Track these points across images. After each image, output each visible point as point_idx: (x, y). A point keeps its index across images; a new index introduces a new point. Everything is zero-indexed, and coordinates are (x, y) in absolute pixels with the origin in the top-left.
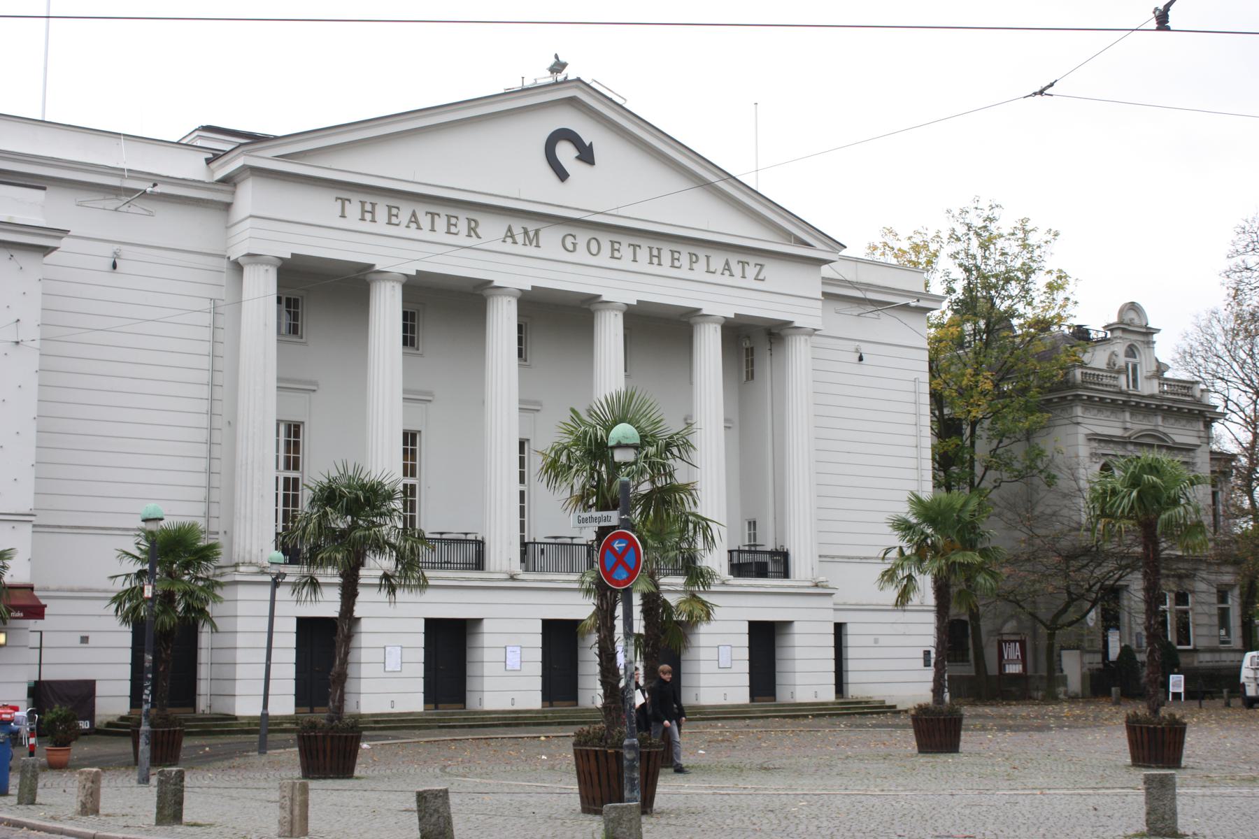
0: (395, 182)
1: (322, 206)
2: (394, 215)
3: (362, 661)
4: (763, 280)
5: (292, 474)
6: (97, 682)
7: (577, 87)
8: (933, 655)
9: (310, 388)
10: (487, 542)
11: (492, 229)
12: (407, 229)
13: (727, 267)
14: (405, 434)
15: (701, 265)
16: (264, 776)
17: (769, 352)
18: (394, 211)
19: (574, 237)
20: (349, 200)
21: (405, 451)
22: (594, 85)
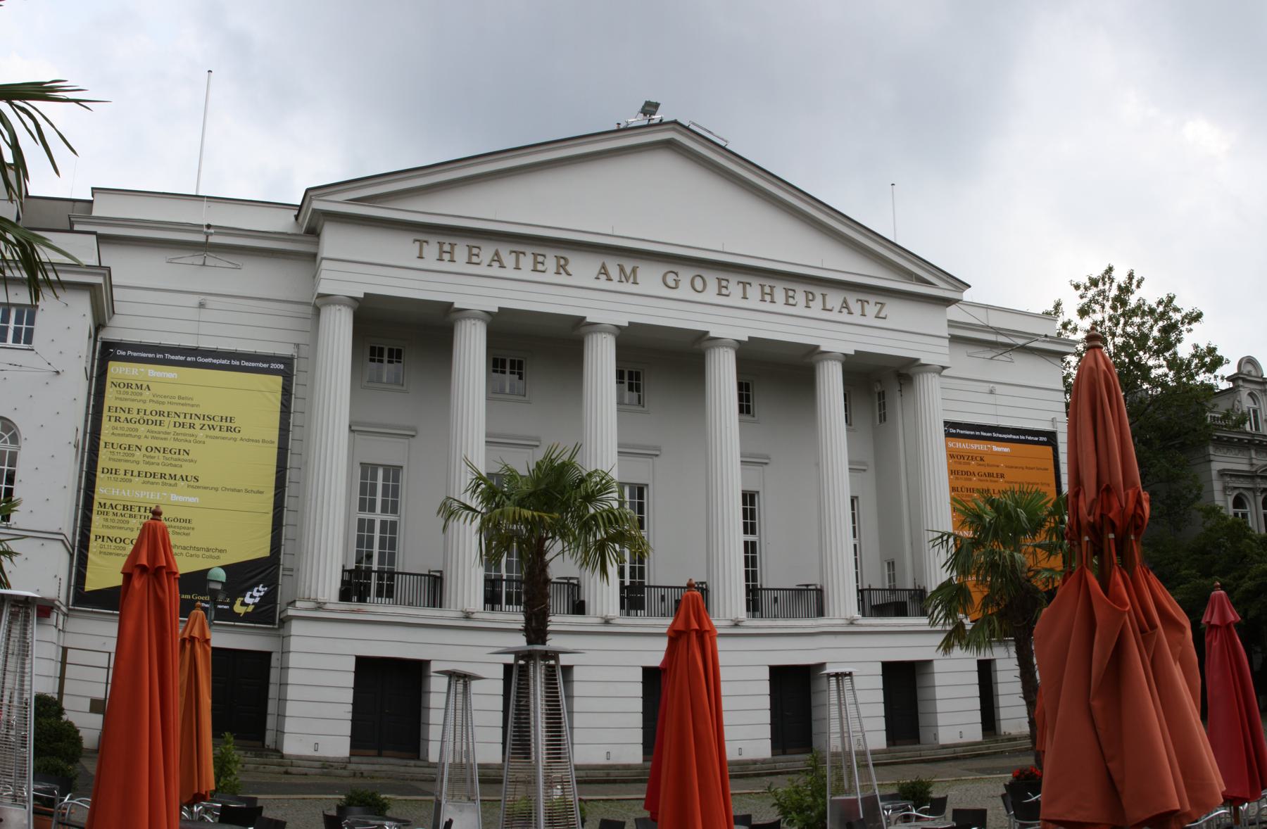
0: (780, 264)
1: (401, 249)
2: (539, 263)
4: (885, 318)
5: (750, 538)
6: (88, 710)
9: (651, 454)
10: (825, 590)
11: (583, 269)
12: (490, 268)
13: (845, 305)
14: (744, 495)
15: (817, 304)
18: (724, 283)
19: (676, 274)
20: (750, 284)
21: (745, 511)
22: (692, 127)
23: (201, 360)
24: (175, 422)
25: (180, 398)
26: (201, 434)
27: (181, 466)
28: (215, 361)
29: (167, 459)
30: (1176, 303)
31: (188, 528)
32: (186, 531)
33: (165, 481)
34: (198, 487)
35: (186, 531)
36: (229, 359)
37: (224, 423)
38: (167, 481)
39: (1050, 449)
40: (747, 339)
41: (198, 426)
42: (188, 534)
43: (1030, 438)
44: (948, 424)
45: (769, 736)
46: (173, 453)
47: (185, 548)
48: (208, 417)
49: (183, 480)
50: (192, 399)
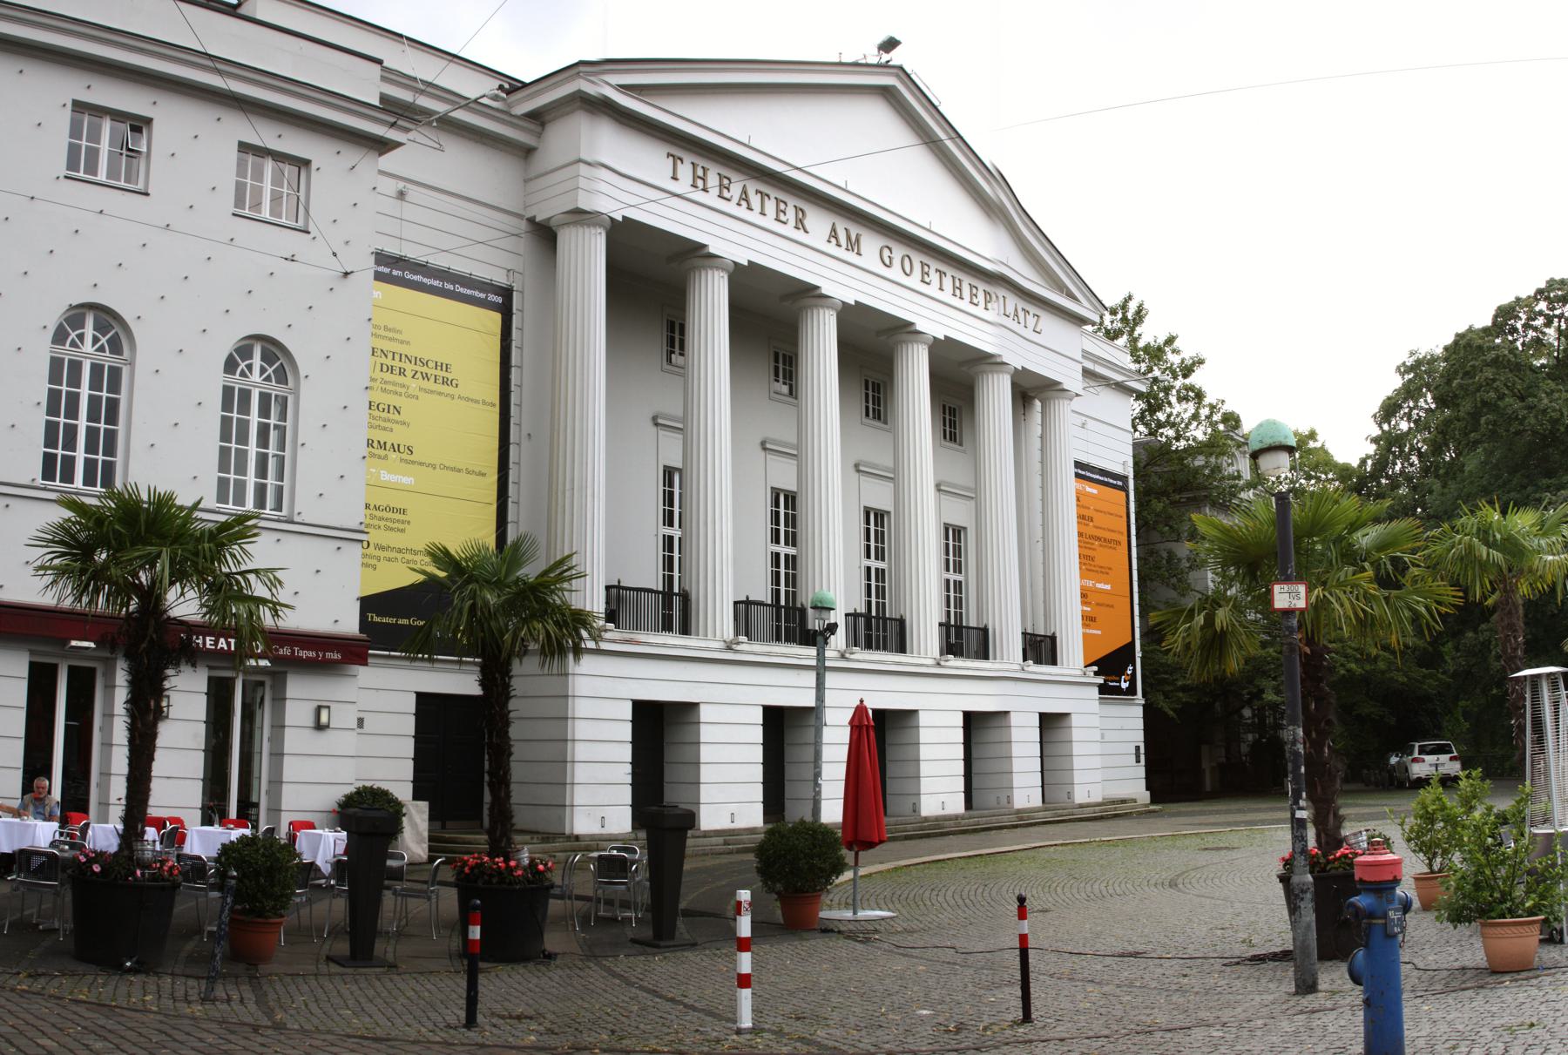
1: (650, 160)
3: (112, 772)
7: (897, 76)
8: (1142, 750)
16: (983, 864)
22: (913, 77)
23: (409, 277)
25: (386, 328)
26: (414, 385)
27: (392, 430)
28: (425, 280)
29: (374, 418)
30: (1176, 344)
31: (403, 522)
33: (373, 450)
34: (413, 462)
37: (438, 372)
39: (1124, 494)
41: (409, 373)
42: (403, 531)
43: (1111, 481)
44: (1078, 464)
45: (761, 798)
46: (381, 409)
47: (400, 551)
50: (400, 332)
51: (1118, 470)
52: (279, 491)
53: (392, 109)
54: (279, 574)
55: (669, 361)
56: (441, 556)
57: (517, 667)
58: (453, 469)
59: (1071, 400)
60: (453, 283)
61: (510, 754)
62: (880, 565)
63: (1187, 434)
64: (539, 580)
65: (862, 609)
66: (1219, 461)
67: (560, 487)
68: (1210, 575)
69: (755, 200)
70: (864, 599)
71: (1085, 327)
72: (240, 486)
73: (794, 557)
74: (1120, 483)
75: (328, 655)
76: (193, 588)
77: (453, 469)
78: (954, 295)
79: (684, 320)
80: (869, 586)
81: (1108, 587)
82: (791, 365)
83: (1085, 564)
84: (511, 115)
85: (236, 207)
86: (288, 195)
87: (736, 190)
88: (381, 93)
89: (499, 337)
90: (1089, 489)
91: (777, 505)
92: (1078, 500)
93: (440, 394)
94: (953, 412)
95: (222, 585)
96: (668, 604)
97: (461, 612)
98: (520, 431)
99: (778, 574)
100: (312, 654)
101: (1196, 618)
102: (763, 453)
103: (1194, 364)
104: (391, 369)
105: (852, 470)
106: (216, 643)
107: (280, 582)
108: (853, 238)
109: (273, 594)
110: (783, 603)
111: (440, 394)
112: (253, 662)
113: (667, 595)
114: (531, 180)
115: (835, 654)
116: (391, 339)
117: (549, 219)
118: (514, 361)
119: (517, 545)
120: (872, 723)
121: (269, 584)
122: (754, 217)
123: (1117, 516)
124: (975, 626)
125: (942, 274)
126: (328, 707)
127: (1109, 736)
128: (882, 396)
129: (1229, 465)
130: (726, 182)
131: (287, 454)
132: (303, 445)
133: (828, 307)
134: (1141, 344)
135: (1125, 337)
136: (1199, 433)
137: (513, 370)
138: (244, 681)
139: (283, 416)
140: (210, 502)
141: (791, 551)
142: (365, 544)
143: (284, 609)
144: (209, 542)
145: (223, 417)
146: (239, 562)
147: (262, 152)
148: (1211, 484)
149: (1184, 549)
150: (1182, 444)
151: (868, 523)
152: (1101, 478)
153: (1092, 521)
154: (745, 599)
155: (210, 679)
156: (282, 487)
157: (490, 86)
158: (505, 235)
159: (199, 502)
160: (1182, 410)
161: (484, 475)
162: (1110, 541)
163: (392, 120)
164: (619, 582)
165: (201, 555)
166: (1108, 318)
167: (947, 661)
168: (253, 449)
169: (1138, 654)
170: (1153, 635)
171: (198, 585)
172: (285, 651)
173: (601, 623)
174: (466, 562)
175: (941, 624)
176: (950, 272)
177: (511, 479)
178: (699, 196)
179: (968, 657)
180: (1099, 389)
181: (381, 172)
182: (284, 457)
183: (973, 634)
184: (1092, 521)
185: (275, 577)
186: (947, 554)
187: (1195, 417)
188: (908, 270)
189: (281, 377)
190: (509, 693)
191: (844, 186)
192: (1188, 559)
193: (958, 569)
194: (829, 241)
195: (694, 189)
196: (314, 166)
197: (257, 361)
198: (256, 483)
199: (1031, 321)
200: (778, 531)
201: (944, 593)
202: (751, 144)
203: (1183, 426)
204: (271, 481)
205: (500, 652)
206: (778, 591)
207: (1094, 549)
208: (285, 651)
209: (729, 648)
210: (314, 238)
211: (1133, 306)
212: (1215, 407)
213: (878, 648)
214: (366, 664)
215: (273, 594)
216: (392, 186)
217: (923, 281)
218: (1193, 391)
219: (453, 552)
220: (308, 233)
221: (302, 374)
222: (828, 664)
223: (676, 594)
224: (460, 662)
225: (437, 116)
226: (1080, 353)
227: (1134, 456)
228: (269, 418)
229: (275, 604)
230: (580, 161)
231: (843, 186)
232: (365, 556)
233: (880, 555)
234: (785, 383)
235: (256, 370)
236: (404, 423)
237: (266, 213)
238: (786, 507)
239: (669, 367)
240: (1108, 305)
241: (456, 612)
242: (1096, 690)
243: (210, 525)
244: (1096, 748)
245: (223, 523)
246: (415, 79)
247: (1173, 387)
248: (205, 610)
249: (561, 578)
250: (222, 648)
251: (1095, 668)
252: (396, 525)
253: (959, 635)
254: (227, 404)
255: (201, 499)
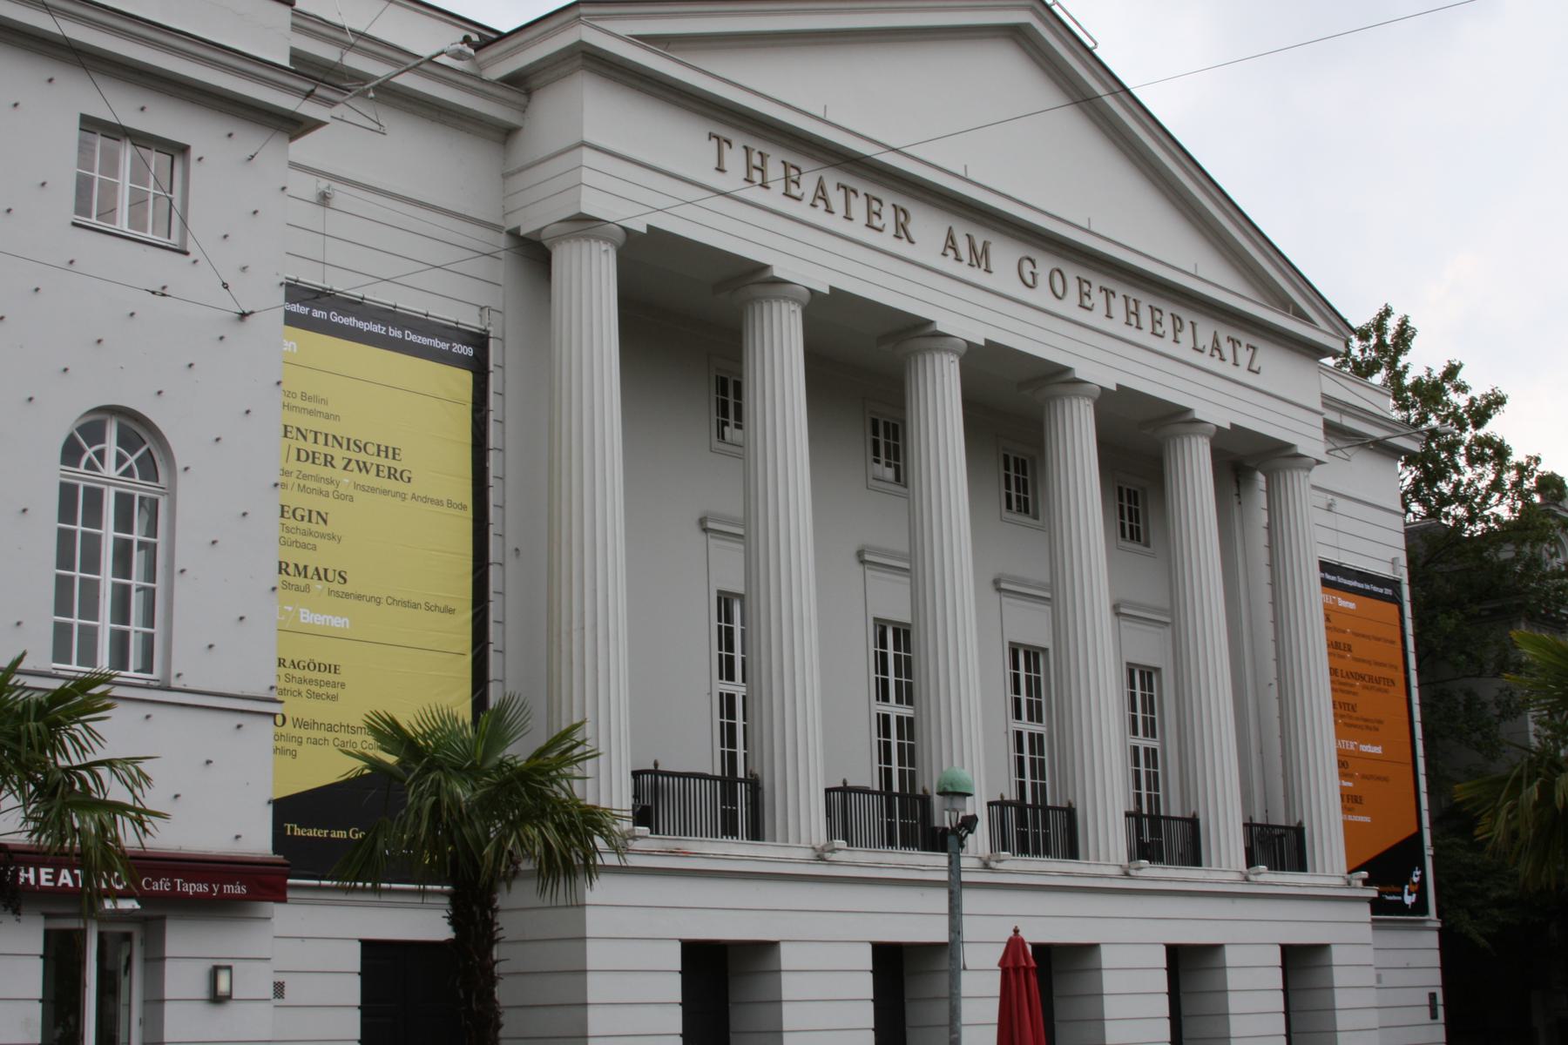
8: (1440, 1000)
17: (1235, 499)
22: (1056, 8)
23: (336, 319)
24: (299, 450)
25: (304, 396)
26: (346, 480)
27: (314, 548)
28: (360, 324)
29: (289, 530)
30: (1461, 376)
31: (334, 685)
32: (332, 691)
34: (347, 596)
35: (332, 691)
36: (385, 323)
37: (382, 461)
38: (291, 580)
39: (1395, 608)
40: (982, 343)
42: (334, 698)
43: (1375, 589)
44: (1325, 566)
47: (331, 728)
48: (355, 443)
49: (320, 579)
50: (324, 401)
51: (1384, 570)
52: (148, 641)
53: (305, 69)
54: (145, 767)
55: (721, 436)
56: (389, 732)
57: (502, 899)
58: (406, 604)
59: (1309, 470)
60: (402, 328)
61: (499, 1026)
62: (1037, 728)
63: (1486, 513)
64: (534, 763)
65: (1012, 795)
66: (1536, 551)
67: (564, 627)
68: (1532, 727)
69: (836, 198)
70: (1014, 779)
71: (1323, 361)
72: (89, 635)
73: (910, 721)
74: (1388, 592)
75: (228, 888)
76: (13, 792)
77: (406, 604)
78: (1128, 323)
79: (741, 375)
80: (1020, 761)
81: (1377, 750)
82: (896, 438)
83: (1342, 716)
84: (483, 81)
85: (77, 213)
86: (156, 197)
87: (808, 185)
88: (293, 50)
89: (470, 406)
90: (1342, 603)
91: (883, 644)
92: (1328, 619)
93: (385, 492)
94: (1133, 496)
95: (58, 784)
96: (729, 796)
97: (418, 814)
98: (504, 545)
99: (887, 746)
100: (202, 888)
101: (1525, 792)
102: (860, 568)
103: (1489, 405)
104: (311, 457)
105: (991, 590)
106: (56, 877)
107: (147, 779)
108: (979, 249)
109: (135, 797)
110: (896, 788)
111: (385, 492)
112: (108, 904)
113: (728, 782)
114: (512, 174)
115: (975, 863)
116: (311, 412)
117: (540, 230)
118: (492, 442)
119: (503, 707)
120: (1033, 964)
121: (129, 782)
122: (836, 223)
123: (1386, 641)
124: (1179, 815)
125: (1109, 293)
126: (229, 968)
127: (1390, 978)
128: (1029, 478)
129: (1552, 556)
130: (793, 172)
131: (159, 585)
132: (182, 571)
133: (947, 351)
134: (1408, 381)
135: (1384, 372)
136: (1503, 509)
137: (492, 454)
138: (101, 936)
139: (152, 530)
140: (40, 657)
141: (906, 711)
142: (279, 720)
143: (153, 819)
144: (35, 720)
145: (60, 530)
146: (83, 748)
147: (117, 132)
148: (1526, 586)
149: (1488, 689)
150: (1479, 527)
151: (1016, 666)
152: (1360, 586)
153: (1350, 650)
154: (841, 785)
155: (48, 934)
156: (152, 635)
157: (448, 38)
158: (477, 254)
159: (20, 660)
160: (1476, 476)
161: (451, 611)
162: (1378, 680)
163: (308, 87)
164: (656, 765)
165: (25, 741)
166: (1356, 345)
167: (1139, 869)
168: (107, 578)
169: (1429, 852)
170: (1453, 820)
171: (21, 787)
172: (162, 885)
173: (627, 825)
174: (425, 739)
175: (1128, 815)
176: (1121, 290)
177: (492, 617)
178: (755, 194)
179: (1170, 862)
180: (1349, 451)
181: (294, 165)
182: (154, 590)
183: (1176, 828)
184: (1350, 650)
185: (139, 772)
186: (1134, 708)
187: (1497, 485)
188: (1059, 290)
189: (149, 469)
190: (493, 934)
191: (963, 174)
192: (1498, 703)
193: (1150, 731)
194: (944, 254)
195: (748, 184)
196: (194, 154)
197: (111, 446)
198: (113, 631)
199: (1244, 355)
200: (885, 683)
201: (1131, 768)
202: (828, 118)
203: (1478, 500)
204: (135, 627)
205: (477, 871)
206: (888, 772)
207: (1355, 694)
208: (162, 885)
209: (820, 858)
210: (195, 262)
211: (1392, 324)
212: (1525, 469)
213: (1036, 852)
214: (283, 900)
215: (135, 797)
216: (309, 186)
217: (1082, 306)
218: (1490, 447)
219: (405, 726)
220: (186, 253)
221: (180, 465)
222: (965, 877)
223: (741, 781)
224: (424, 893)
225: (375, 83)
226: (1319, 400)
227: (1408, 550)
228: (130, 531)
229: (140, 812)
230: (583, 144)
231: (961, 172)
232: (278, 737)
233: (1035, 714)
234: (888, 465)
235: (111, 458)
236: (332, 537)
237: (122, 224)
238: (897, 647)
239: (721, 446)
240: (1355, 325)
241: (412, 816)
242: (1367, 908)
243: (36, 695)
244: (1371, 998)
245: (56, 692)
246: (342, 29)
247: (1460, 443)
248: (31, 825)
249: (566, 759)
250: (65, 885)
251: (1365, 874)
252: (324, 690)
253: (1155, 830)
254: (66, 511)
255: (24, 654)
